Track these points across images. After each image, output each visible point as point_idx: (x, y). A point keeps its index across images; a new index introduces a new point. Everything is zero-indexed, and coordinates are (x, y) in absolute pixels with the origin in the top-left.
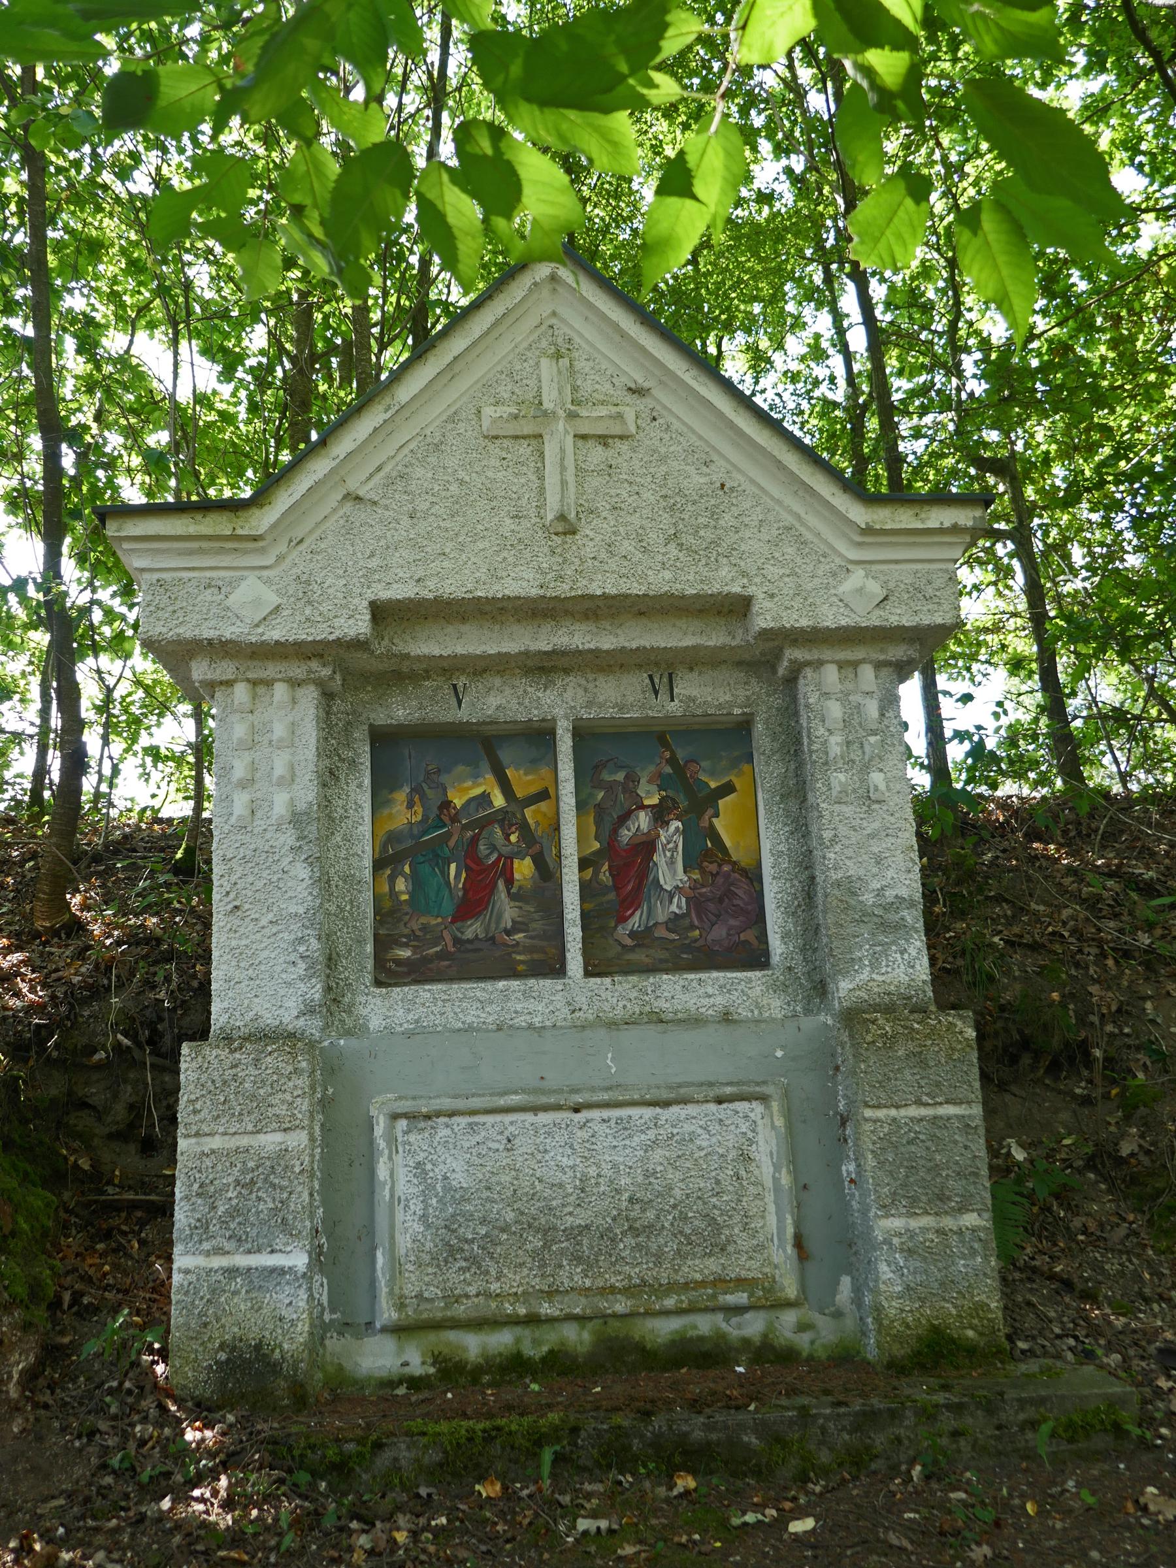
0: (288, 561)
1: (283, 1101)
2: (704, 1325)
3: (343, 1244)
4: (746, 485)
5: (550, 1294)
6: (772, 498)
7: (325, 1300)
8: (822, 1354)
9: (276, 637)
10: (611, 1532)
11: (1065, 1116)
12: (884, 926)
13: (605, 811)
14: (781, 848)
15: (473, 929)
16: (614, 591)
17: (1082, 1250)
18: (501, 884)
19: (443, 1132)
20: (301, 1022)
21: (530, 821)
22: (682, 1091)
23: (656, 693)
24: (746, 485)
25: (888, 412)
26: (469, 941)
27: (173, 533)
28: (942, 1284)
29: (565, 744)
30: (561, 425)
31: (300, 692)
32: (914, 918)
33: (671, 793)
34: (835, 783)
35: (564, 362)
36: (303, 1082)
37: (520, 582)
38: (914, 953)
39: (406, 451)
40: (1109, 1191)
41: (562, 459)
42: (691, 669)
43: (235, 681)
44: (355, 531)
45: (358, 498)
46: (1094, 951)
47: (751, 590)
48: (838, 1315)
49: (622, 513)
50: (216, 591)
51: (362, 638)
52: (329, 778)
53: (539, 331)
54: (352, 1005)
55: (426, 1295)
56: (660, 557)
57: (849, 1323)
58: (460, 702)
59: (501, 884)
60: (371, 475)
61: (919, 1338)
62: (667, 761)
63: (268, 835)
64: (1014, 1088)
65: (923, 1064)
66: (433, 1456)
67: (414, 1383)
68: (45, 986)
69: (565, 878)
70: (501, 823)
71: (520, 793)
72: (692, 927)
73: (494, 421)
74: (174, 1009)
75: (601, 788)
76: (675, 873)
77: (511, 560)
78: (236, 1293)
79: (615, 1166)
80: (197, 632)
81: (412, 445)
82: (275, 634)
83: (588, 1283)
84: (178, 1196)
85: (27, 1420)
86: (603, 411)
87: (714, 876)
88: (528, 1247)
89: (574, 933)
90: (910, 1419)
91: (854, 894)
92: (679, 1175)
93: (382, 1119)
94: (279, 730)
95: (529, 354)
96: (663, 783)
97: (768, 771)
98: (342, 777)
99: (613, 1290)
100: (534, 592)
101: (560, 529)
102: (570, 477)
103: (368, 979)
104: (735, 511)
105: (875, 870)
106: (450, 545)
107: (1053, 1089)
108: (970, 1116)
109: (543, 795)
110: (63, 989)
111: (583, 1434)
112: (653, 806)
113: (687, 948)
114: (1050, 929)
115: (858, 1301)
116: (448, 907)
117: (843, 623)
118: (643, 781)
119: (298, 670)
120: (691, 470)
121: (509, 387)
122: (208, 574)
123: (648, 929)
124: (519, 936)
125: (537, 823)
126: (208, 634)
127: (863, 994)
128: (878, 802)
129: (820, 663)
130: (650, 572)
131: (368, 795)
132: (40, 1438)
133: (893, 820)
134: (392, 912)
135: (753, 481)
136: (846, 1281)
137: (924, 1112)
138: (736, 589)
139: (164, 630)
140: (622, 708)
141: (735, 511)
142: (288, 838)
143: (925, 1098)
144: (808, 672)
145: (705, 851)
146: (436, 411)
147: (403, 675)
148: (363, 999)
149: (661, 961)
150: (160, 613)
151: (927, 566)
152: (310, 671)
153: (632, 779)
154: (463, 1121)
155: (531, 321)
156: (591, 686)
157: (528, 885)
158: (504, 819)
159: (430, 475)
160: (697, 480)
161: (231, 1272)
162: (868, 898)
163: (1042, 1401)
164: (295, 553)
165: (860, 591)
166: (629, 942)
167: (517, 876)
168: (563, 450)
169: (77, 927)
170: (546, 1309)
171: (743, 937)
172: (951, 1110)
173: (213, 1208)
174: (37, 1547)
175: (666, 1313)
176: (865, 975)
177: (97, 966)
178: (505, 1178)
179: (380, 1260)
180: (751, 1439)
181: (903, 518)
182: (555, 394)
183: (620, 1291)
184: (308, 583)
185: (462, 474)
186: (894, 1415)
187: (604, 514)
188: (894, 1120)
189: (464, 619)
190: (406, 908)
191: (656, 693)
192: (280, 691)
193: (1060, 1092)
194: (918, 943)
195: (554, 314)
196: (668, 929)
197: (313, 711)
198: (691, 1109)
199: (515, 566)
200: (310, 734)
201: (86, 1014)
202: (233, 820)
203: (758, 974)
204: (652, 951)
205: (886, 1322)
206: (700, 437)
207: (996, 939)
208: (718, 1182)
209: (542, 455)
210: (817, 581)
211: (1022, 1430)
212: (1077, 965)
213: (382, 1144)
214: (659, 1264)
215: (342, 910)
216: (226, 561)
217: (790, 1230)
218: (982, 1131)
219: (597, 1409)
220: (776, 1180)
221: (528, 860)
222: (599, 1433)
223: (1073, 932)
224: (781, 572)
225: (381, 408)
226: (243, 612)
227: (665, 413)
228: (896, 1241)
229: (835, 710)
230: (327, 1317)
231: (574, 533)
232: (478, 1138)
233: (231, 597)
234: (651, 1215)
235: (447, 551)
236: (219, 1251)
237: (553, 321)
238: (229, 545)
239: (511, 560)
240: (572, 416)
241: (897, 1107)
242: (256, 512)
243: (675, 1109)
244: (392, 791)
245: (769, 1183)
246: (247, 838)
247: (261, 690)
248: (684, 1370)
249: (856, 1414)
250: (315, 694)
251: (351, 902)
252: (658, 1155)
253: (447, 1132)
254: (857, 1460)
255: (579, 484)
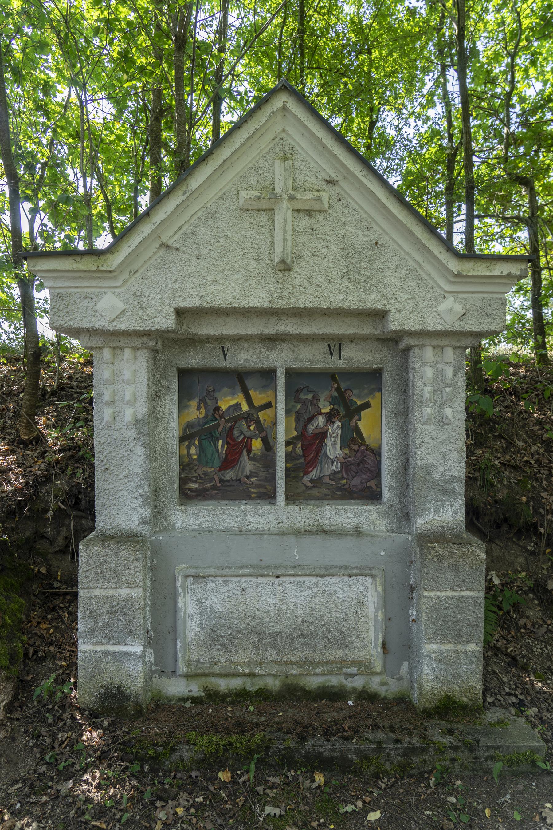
0: (129, 283)
1: (130, 574)
2: (335, 681)
3: (162, 633)
4: (390, 243)
5: (260, 664)
6: (405, 251)
7: (152, 660)
8: (391, 696)
9: (123, 328)
10: (281, 816)
11: (521, 559)
12: (444, 491)
13: (302, 417)
14: (393, 442)
15: (230, 475)
16: (311, 306)
17: (523, 637)
18: (245, 452)
19: (210, 585)
20: (140, 528)
21: (261, 419)
22: (332, 571)
23: (331, 354)
24: (390, 243)
25: (470, 153)
26: (227, 481)
27: (64, 268)
28: (454, 677)
29: (281, 381)
30: (285, 204)
31: (139, 353)
32: (459, 487)
33: (336, 406)
34: (425, 414)
35: (289, 163)
36: (139, 564)
37: (258, 299)
38: (458, 506)
39: (195, 217)
40: (539, 605)
41: (285, 226)
42: (352, 341)
43: (104, 347)
44: (166, 266)
45: (168, 247)
46: (546, 472)
47: (388, 307)
48: (400, 679)
49: (318, 259)
50: (90, 300)
51: (170, 329)
52: (155, 397)
53: (275, 141)
54: (167, 515)
55: (201, 660)
56: (337, 286)
57: (405, 683)
58: (225, 356)
59: (245, 452)
60: (176, 232)
61: (440, 700)
62: (336, 389)
63: (122, 431)
64: (497, 541)
65: (457, 571)
66: (199, 756)
67: (195, 700)
68: (24, 476)
69: (278, 454)
70: (246, 419)
71: (257, 404)
72: (343, 478)
73: (246, 200)
74: (87, 488)
75: (299, 403)
76: (336, 450)
77: (254, 285)
78: (108, 663)
79: (295, 605)
80: (80, 324)
81: (199, 214)
82: (122, 326)
83: (279, 659)
84: (79, 617)
85: (7, 731)
86: (309, 195)
87: (356, 452)
88: (251, 641)
89: (281, 482)
90: (432, 752)
91: (430, 474)
92: (327, 610)
93: (180, 578)
94: (128, 375)
95: (268, 157)
96: (333, 401)
97: (388, 399)
98: (162, 396)
99: (292, 663)
100: (266, 305)
101: (282, 268)
102: (289, 237)
103: (175, 501)
104: (383, 259)
105: (442, 461)
106: (219, 275)
107: (516, 544)
108: (477, 597)
109: (268, 405)
110: (32, 478)
111: (271, 750)
112: (326, 414)
113: (339, 489)
114: (525, 459)
115: (411, 674)
116: (217, 463)
117: (439, 328)
118: (322, 399)
119: (137, 343)
120: (359, 232)
121: (256, 178)
122: (86, 290)
123: (320, 479)
124: (253, 479)
125: (265, 420)
126: (86, 325)
127: (429, 526)
128: (447, 424)
129: (424, 346)
130: (332, 295)
131: (177, 406)
132: (14, 739)
133: (454, 434)
134: (188, 464)
135: (393, 240)
136: (406, 664)
137: (454, 594)
138: (380, 306)
139: (63, 323)
140: (312, 362)
141: (383, 259)
142: (132, 433)
143: (455, 588)
144: (416, 350)
145: (352, 438)
146: (213, 193)
147: (194, 342)
148: (173, 512)
149: (326, 495)
150: (60, 313)
151: (490, 296)
152: (143, 343)
153: (316, 398)
154: (221, 579)
155: (270, 136)
156: (296, 349)
157: (259, 453)
158: (248, 417)
159: (209, 233)
160: (361, 239)
161: (106, 653)
162: (437, 476)
163: (498, 747)
164: (133, 279)
165: (450, 310)
166: (309, 484)
167: (253, 448)
168: (285, 220)
169: (39, 440)
170: (258, 671)
171: (368, 484)
172: (469, 594)
173: (96, 623)
174: (6, 818)
175: (317, 675)
176: (431, 517)
177: (49, 464)
178: (241, 608)
179: (179, 645)
180: (353, 757)
181: (480, 268)
182: (282, 184)
183: (294, 663)
184: (140, 296)
185: (227, 232)
186: (424, 750)
187: (307, 259)
188: (439, 598)
189: (227, 315)
190: (196, 463)
191: (331, 354)
192: (128, 353)
193: (520, 546)
194: (460, 501)
195: (284, 130)
196: (330, 479)
197: (145, 363)
198: (335, 579)
199: (256, 289)
200: (144, 377)
201: (43, 491)
202: (104, 423)
203: (375, 507)
204: (321, 490)
205: (424, 692)
206: (366, 212)
207: (497, 462)
208: (346, 615)
209: (273, 221)
210: (426, 303)
211: (486, 760)
212: (537, 480)
213: (180, 590)
214: (314, 651)
215: (162, 466)
216: (95, 283)
217: (380, 641)
218: (483, 605)
219: (280, 729)
220: (375, 617)
221: (259, 440)
222: (279, 750)
223: (537, 461)
224: (406, 296)
225: (181, 192)
226: (104, 314)
227: (346, 196)
228: (433, 655)
229: (429, 372)
230: (153, 668)
231: (290, 270)
232: (228, 588)
233: (98, 304)
234: (312, 628)
235: (218, 279)
236: (99, 643)
237: (283, 135)
238: (96, 275)
239: (254, 285)
240: (292, 198)
241: (441, 591)
242: (110, 256)
243: (327, 578)
244: (189, 401)
245: (372, 616)
246: (111, 432)
247: (118, 351)
248: (323, 701)
249: (405, 748)
250: (146, 355)
251: (167, 462)
252: (317, 600)
253: (213, 584)
254: (404, 768)
255: (294, 240)
